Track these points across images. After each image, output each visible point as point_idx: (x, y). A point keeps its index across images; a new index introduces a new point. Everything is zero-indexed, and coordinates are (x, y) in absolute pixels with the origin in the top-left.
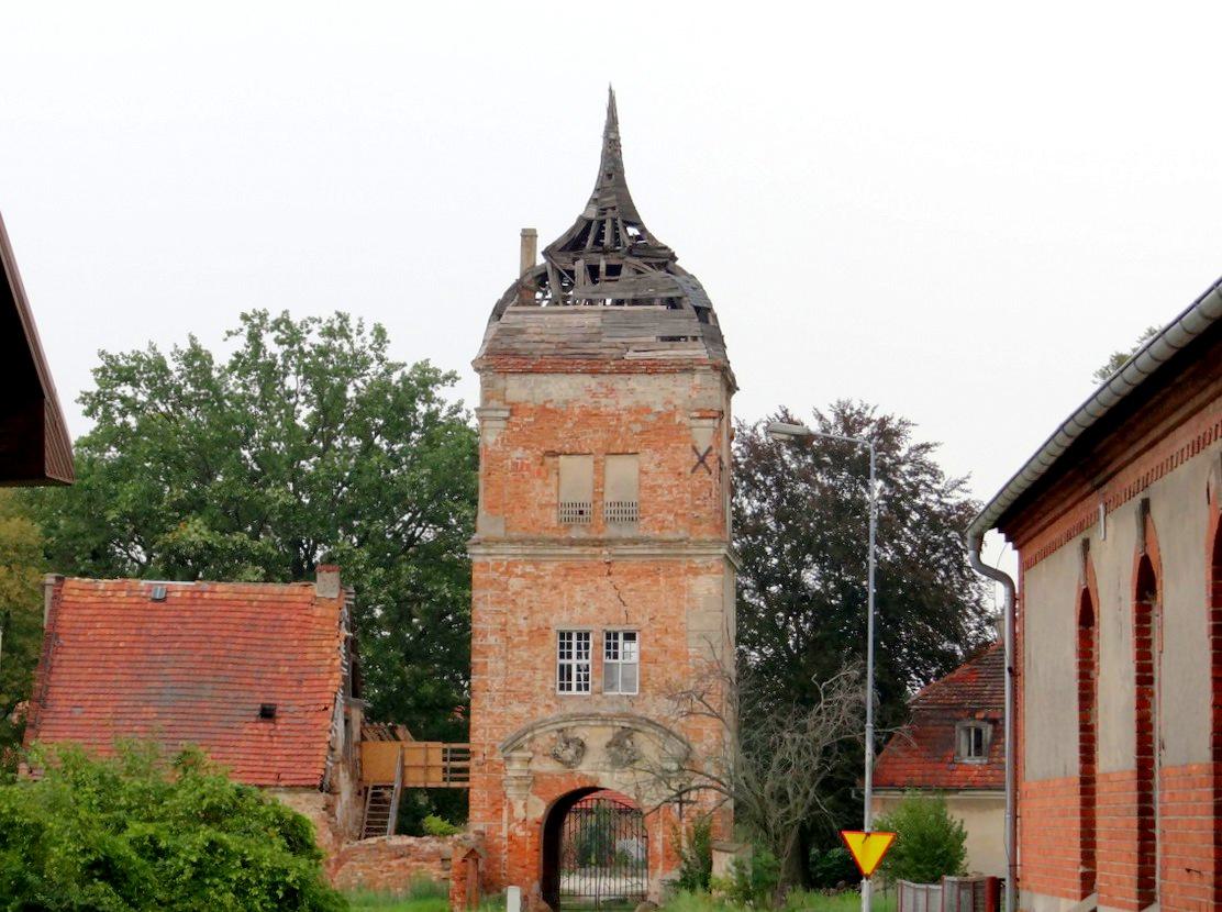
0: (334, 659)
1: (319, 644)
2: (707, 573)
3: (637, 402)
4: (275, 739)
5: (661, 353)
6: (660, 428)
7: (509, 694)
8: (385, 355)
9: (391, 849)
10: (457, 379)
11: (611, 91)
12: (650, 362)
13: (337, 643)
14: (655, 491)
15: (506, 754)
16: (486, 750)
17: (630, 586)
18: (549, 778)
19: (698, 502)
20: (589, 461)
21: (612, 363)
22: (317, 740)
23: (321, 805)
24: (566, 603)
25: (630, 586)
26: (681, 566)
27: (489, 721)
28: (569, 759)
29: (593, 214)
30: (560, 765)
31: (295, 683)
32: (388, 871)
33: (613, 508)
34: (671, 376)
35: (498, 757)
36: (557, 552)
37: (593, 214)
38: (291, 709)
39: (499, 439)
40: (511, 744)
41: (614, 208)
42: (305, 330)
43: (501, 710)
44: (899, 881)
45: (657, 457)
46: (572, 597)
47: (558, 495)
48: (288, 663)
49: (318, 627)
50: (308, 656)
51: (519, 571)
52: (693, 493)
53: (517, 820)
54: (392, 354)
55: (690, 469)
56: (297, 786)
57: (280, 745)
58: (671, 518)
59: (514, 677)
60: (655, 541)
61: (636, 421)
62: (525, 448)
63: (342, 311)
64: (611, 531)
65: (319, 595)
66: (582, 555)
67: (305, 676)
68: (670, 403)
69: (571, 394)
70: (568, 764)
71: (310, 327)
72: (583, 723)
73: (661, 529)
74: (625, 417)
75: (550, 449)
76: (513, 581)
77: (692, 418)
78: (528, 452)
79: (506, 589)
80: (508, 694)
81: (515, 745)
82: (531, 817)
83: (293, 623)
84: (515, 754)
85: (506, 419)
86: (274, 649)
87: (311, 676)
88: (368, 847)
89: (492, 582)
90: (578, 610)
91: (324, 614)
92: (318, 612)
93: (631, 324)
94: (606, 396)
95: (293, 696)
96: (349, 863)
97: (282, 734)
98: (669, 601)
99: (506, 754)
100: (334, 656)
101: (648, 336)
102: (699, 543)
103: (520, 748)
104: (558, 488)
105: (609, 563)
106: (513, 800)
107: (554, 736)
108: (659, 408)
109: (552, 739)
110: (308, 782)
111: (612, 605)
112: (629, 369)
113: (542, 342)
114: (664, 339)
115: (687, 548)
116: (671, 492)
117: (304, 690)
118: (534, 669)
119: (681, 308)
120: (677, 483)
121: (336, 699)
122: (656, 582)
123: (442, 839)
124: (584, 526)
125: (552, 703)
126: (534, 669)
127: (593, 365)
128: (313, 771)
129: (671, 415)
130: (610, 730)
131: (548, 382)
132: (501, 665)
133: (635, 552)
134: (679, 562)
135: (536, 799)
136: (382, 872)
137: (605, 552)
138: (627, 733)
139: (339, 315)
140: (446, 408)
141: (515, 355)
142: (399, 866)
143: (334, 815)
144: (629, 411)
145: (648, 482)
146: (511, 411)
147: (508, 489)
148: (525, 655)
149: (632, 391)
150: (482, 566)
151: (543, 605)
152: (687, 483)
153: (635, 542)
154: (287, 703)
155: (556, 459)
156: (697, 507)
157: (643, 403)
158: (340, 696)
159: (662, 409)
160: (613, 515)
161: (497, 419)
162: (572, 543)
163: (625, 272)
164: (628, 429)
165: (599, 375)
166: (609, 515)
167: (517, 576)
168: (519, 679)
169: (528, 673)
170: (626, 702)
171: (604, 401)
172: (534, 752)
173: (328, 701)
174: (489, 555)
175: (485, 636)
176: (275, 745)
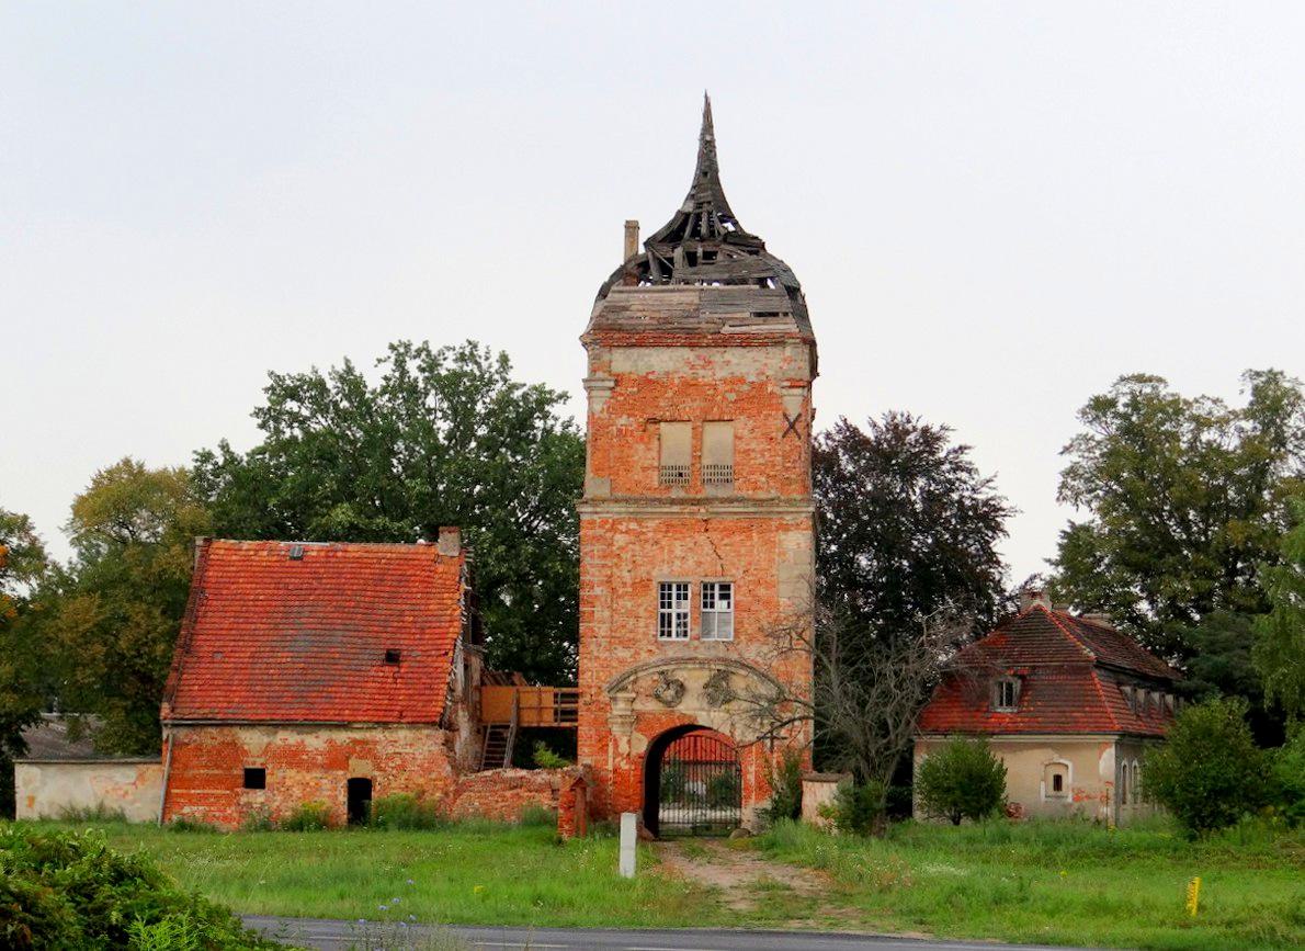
4: (399, 681)
5: (754, 327)
6: (754, 397)
7: (615, 640)
8: (508, 377)
9: (504, 781)
13: (457, 596)
16: (593, 691)
17: (726, 541)
19: (789, 465)
20: (688, 428)
21: (710, 337)
28: (669, 699)
29: (690, 208)
31: (418, 631)
34: (764, 349)
35: (605, 697)
36: (658, 510)
37: (690, 208)
38: (414, 654)
39: (605, 407)
41: (709, 203)
42: (442, 357)
43: (607, 654)
44: (412, 795)
45: (751, 423)
49: (440, 581)
50: (431, 607)
51: (623, 528)
54: (514, 376)
55: (781, 434)
56: (418, 723)
58: (763, 479)
60: (748, 500)
62: (629, 416)
63: (472, 339)
64: (709, 491)
65: (441, 554)
67: (428, 625)
68: (763, 374)
69: (670, 366)
70: (668, 704)
74: (721, 387)
76: (618, 537)
78: (631, 419)
79: (611, 544)
81: (620, 686)
82: (634, 753)
84: (619, 695)
85: (612, 389)
89: (598, 539)
90: (678, 563)
92: (441, 568)
94: (703, 367)
100: (454, 607)
102: (789, 502)
103: (624, 689)
104: (659, 452)
107: (656, 677)
108: (752, 378)
110: (427, 719)
111: (709, 559)
112: (724, 342)
114: (759, 315)
116: (763, 456)
121: (455, 645)
122: (750, 538)
125: (653, 648)
127: (693, 339)
128: (433, 709)
129: (762, 385)
130: (707, 673)
131: (650, 355)
132: (607, 613)
133: (731, 510)
135: (640, 736)
136: (497, 801)
138: (723, 676)
139: (470, 343)
141: (619, 330)
144: (724, 381)
145: (742, 446)
147: (614, 453)
148: (629, 604)
149: (728, 363)
152: (778, 447)
153: (731, 501)
155: (657, 426)
156: (787, 469)
157: (737, 374)
158: (459, 643)
161: (604, 389)
162: (673, 502)
163: (720, 257)
167: (622, 532)
168: (624, 626)
169: (632, 621)
170: (722, 647)
171: (701, 372)
174: (596, 513)
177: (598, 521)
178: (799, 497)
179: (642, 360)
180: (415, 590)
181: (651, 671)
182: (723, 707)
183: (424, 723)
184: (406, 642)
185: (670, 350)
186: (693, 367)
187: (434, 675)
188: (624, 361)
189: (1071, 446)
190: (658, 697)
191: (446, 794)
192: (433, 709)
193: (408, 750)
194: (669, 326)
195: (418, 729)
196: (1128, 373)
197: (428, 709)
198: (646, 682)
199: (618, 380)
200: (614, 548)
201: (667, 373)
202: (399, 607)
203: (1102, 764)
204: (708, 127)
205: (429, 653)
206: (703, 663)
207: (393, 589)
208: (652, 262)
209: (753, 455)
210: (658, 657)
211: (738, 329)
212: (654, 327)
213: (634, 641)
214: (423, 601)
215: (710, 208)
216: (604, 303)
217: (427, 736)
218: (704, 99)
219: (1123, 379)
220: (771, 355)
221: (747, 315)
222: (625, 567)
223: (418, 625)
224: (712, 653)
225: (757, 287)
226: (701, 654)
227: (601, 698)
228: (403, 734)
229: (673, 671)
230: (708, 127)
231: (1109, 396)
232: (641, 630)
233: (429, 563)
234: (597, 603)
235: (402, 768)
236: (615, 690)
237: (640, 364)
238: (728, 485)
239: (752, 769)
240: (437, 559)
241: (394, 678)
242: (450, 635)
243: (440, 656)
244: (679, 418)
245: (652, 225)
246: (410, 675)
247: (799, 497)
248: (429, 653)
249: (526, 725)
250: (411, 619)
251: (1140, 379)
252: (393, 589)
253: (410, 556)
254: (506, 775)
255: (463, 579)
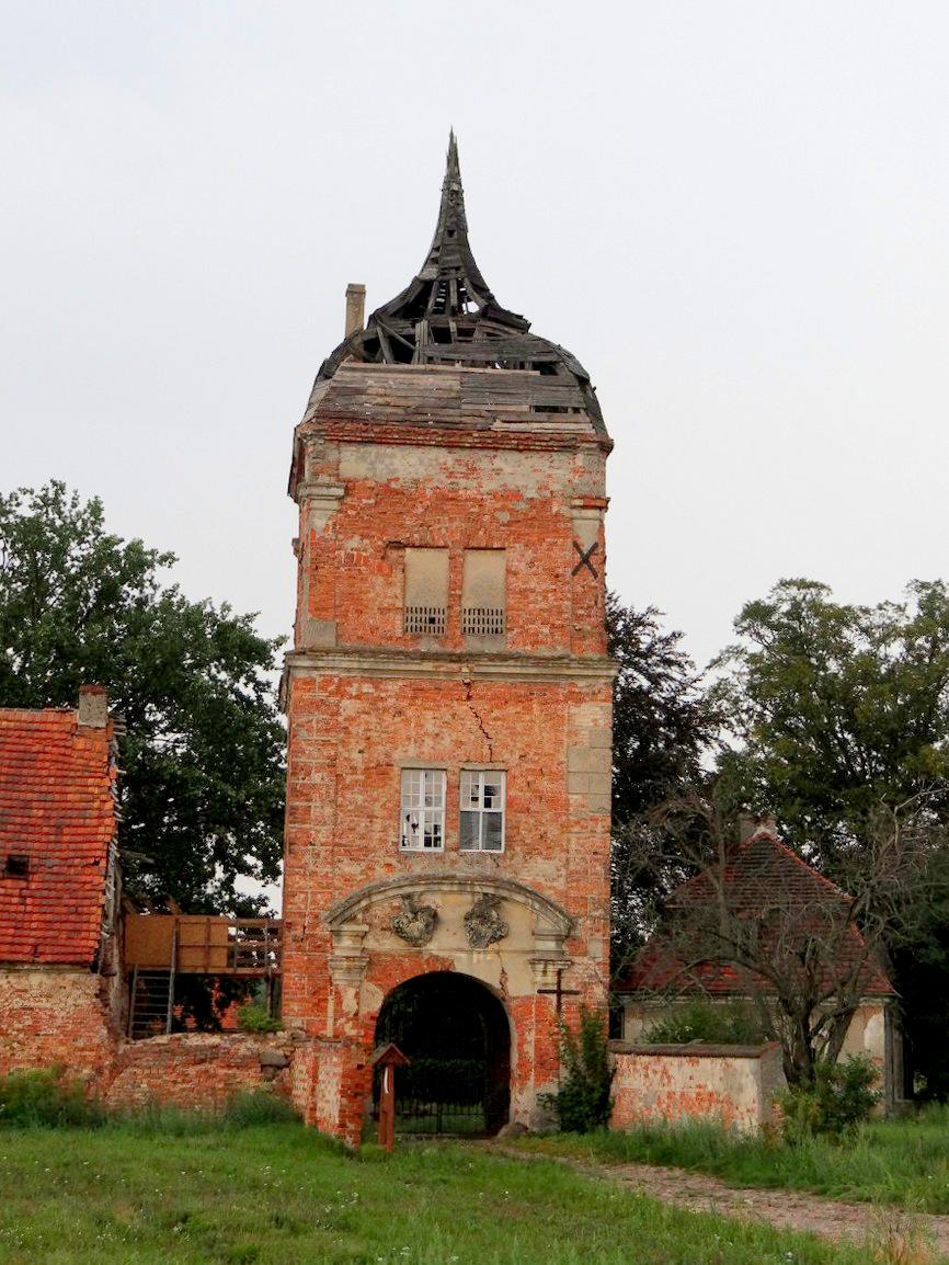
0: (105, 801)
1: (82, 781)
2: (592, 700)
3: (505, 485)
4: (29, 901)
5: (536, 425)
6: (533, 518)
7: (339, 849)
8: (102, 529)
9: (188, 1051)
10: (174, 559)
11: (452, 135)
12: (522, 436)
13: (107, 782)
14: (527, 597)
15: (335, 927)
16: (307, 921)
17: (496, 713)
18: (389, 959)
19: (580, 612)
20: (444, 556)
21: (475, 435)
22: (87, 902)
23: (93, 991)
24: (414, 733)
25: (496, 713)
26: (561, 691)
27: (311, 884)
28: (416, 934)
29: (432, 273)
30: (402, 942)
31: (53, 830)
32: (184, 1081)
33: (472, 617)
34: (547, 455)
35: (323, 930)
36: (403, 667)
37: (432, 273)
38: (49, 863)
39: (330, 523)
40: (342, 913)
41: (458, 269)
42: (14, 503)
43: (328, 869)
44: (46, 1071)
45: (529, 554)
46: (422, 726)
47: (404, 598)
48: (42, 805)
49: (81, 761)
50: (70, 797)
51: (353, 691)
52: (574, 601)
53: (348, 1013)
54: (108, 529)
55: (570, 570)
56: (63, 963)
57: (36, 909)
58: (546, 630)
59: (345, 826)
60: (529, 658)
61: (503, 509)
62: (363, 537)
63: (57, 479)
64: (472, 644)
65: (81, 723)
66: (437, 673)
67: (67, 821)
68: (546, 488)
69: (421, 472)
70: (412, 941)
71: (19, 500)
72: (436, 887)
73: (535, 643)
74: (489, 503)
75: (393, 539)
76: (345, 703)
77: (574, 507)
78: (366, 541)
79: (337, 713)
80: (336, 849)
81: (347, 914)
82: (364, 1011)
83: (48, 757)
84: (345, 927)
85: (340, 499)
86: (24, 787)
87: (74, 822)
88: (157, 1049)
89: (318, 705)
90: (429, 742)
91: (88, 747)
92: (80, 744)
93: (498, 388)
94: (466, 476)
95: (51, 846)
96: (129, 1070)
97: (38, 894)
98: (544, 734)
99: (335, 927)
100: (103, 797)
101: (521, 404)
102: (584, 662)
103: (352, 919)
104: (404, 590)
105: (468, 685)
106: (340, 988)
107: (396, 904)
108: (532, 494)
109: (394, 908)
110: (78, 958)
111: (473, 737)
112: (495, 444)
113: (388, 405)
114: (538, 409)
115: (569, 668)
116: (545, 598)
117: (66, 838)
118: (371, 817)
119: (556, 374)
120: (554, 587)
121: (108, 851)
122: (529, 710)
123: (261, 1038)
124: (437, 637)
125: (393, 861)
126: (371, 817)
127: (451, 436)
128: (83, 943)
129: (546, 503)
130: (469, 897)
131: (392, 456)
132: (328, 810)
133: (504, 670)
134: (557, 685)
135: (371, 986)
136: (175, 1082)
137: (465, 670)
138: (492, 902)
139: (54, 484)
140: (159, 592)
141: (353, 419)
142: (198, 1075)
143: (106, 1005)
144: (494, 495)
145: (518, 584)
146: (346, 489)
147: (341, 587)
148: (360, 798)
149: (498, 472)
150: (306, 683)
151: (383, 736)
152: (567, 588)
153: (504, 657)
154: (42, 855)
155: (400, 553)
156: (579, 618)
157: (512, 487)
158: (114, 848)
159: (535, 496)
160: (472, 625)
161: (328, 498)
162: (424, 657)
163: (477, 335)
164: (493, 517)
165: (457, 450)
166: (467, 625)
167: (351, 697)
168: (351, 830)
169: (364, 823)
170: (489, 861)
171: (463, 482)
172: (370, 925)
173: (99, 853)
174: (316, 668)
175: (309, 774)
176: (29, 908)
177: (319, 680)
178: (596, 656)
179: (383, 462)
180: (44, 772)
181: (390, 893)
182: (491, 946)
183: (70, 963)
184: (36, 845)
185: (421, 450)
186: (451, 475)
187: (80, 894)
188: (355, 462)
189: (720, 659)
190: (399, 931)
191: (99, 1071)
192: (83, 943)
193: (45, 1004)
194: (420, 418)
195: (60, 972)
196: (796, 576)
197: (74, 943)
198: (382, 908)
199: (349, 487)
200: (341, 719)
201: (416, 482)
202: (22, 796)
203: (868, 1034)
204: (453, 176)
205: (70, 862)
206: (463, 884)
207: (13, 771)
208: (383, 338)
209: (532, 597)
210: (402, 874)
211: (513, 427)
212: (400, 418)
213: (366, 850)
214: (58, 789)
215: (460, 275)
216: (326, 385)
217: (74, 983)
218: (449, 139)
219: (785, 584)
220: (555, 464)
221: (525, 408)
222: (356, 745)
223: (52, 822)
224: (476, 870)
225: (537, 373)
226: (462, 871)
227: (318, 931)
228: (37, 980)
229: (422, 894)
230: (453, 176)
231: (768, 602)
232: (378, 836)
233: (64, 736)
234: (315, 796)
235: (34, 1031)
236: (339, 920)
237: (380, 466)
238: (499, 636)
239: (531, 1037)
240: (75, 731)
241: (21, 896)
242: (100, 837)
243: (87, 865)
244: (431, 542)
245: (384, 290)
246: (45, 893)
247: (596, 656)
248: (70, 862)
249: (187, 971)
250: (41, 813)
251: (803, 584)
252: (13, 771)
253: (35, 726)
254: (189, 1042)
255: (113, 759)
